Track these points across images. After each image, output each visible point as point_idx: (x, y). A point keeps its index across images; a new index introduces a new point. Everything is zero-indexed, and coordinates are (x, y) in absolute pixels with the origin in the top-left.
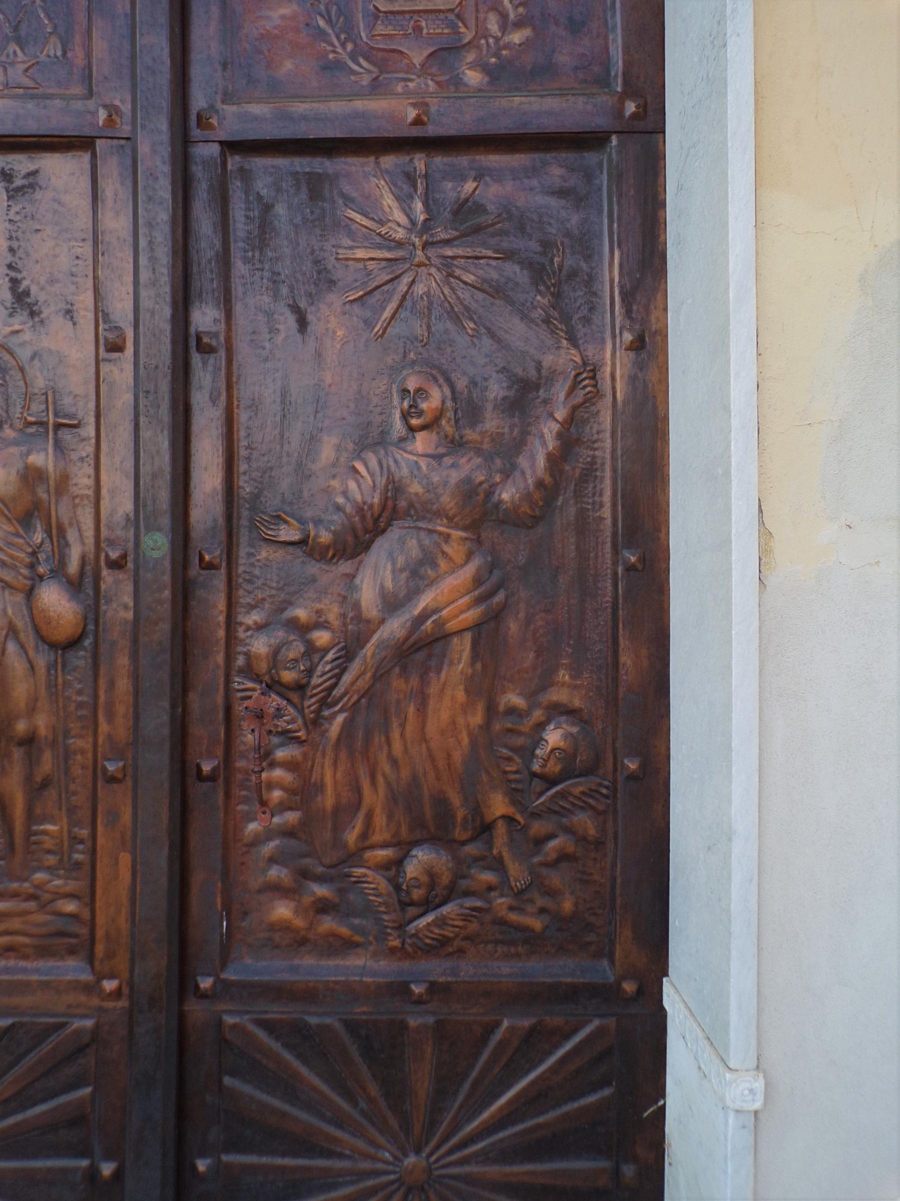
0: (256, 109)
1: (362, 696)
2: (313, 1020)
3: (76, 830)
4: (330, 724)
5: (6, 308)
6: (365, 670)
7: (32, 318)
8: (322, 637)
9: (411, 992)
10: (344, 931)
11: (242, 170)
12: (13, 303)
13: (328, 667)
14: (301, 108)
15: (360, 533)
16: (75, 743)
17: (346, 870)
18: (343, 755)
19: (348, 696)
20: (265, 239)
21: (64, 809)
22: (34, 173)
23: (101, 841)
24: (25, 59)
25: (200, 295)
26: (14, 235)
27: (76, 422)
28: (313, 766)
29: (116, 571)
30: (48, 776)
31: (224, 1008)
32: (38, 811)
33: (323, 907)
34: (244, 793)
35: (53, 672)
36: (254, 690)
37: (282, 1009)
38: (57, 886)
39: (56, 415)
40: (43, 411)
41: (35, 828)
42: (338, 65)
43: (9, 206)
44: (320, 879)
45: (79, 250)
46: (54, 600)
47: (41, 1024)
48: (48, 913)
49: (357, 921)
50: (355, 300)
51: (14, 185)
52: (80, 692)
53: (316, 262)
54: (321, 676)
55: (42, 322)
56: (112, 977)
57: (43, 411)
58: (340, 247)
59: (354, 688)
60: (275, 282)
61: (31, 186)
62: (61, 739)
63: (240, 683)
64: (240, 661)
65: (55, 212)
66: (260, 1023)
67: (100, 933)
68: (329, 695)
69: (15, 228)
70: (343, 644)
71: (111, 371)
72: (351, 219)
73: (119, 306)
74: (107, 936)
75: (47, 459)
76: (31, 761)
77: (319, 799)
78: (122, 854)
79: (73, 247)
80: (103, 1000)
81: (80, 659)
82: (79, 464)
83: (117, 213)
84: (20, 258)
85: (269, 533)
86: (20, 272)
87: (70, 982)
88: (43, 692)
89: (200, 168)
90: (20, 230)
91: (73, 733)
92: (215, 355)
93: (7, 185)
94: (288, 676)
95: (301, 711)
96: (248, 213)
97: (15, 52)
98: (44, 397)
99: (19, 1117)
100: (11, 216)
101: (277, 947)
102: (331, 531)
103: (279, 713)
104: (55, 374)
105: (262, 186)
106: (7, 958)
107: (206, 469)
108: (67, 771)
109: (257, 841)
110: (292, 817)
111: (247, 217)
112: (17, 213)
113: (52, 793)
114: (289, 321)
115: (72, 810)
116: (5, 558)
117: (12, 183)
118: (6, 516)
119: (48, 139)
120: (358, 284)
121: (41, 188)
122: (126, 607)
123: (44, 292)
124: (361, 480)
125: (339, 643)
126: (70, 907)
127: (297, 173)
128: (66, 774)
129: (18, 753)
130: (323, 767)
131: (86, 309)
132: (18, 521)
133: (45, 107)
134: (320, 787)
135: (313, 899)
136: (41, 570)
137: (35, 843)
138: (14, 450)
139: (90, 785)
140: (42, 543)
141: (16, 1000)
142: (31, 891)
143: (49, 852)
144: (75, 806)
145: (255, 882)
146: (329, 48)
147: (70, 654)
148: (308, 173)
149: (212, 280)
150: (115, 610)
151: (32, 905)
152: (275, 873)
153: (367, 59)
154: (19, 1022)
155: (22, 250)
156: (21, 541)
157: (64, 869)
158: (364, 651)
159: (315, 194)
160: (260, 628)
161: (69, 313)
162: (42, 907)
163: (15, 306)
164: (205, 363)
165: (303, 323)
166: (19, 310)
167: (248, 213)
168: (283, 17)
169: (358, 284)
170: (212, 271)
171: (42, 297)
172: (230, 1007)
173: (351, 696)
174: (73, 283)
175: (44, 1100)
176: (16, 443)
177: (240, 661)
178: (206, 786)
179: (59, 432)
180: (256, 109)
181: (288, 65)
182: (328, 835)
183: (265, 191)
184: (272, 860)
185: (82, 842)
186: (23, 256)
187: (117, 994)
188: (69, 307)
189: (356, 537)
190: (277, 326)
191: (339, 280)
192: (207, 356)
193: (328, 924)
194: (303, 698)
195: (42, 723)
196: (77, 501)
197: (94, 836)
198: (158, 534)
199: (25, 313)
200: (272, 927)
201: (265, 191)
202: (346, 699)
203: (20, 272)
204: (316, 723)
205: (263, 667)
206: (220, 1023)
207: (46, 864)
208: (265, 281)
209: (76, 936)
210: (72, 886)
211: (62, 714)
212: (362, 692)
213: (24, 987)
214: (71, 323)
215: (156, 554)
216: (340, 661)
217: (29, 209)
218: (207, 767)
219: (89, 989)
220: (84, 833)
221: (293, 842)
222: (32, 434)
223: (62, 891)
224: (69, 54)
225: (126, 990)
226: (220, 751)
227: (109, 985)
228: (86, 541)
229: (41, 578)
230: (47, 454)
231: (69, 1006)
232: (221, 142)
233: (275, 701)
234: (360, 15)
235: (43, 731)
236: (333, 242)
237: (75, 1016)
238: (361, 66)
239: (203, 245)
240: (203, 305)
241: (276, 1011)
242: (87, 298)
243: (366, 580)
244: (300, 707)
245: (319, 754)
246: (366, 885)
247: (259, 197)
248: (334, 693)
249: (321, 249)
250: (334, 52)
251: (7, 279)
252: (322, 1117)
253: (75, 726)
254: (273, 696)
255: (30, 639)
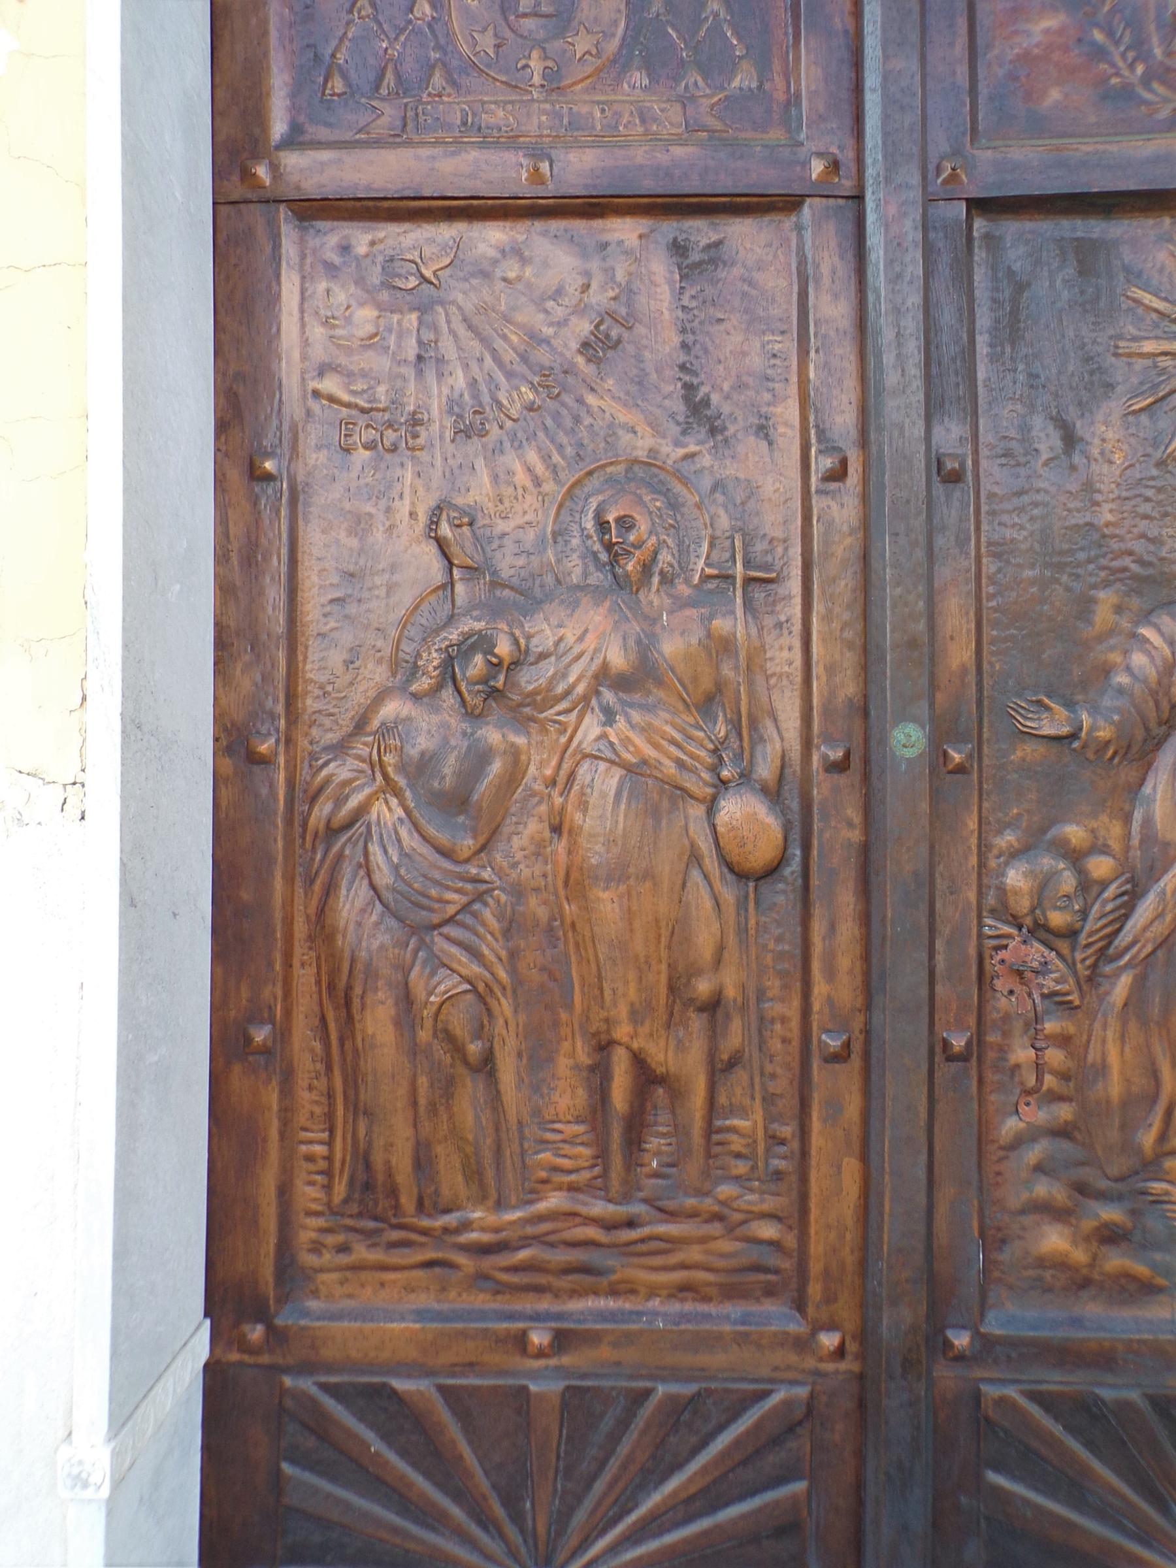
0: (1017, 154)
1: (1160, 945)
2: (1107, 1394)
3: (775, 1126)
4: (1114, 985)
5: (678, 424)
6: (1163, 910)
7: (713, 435)
8: (1100, 866)
9: (948, 1344)
10: (1141, 1269)
11: (987, 237)
12: (687, 417)
13: (1110, 907)
14: (1086, 147)
15: (1152, 724)
16: (772, 1008)
17: (1142, 1184)
18: (1133, 1026)
19: (1139, 945)
20: (1019, 329)
21: (758, 1096)
22: (718, 244)
23: (817, 1140)
24: (708, 91)
25: (942, 405)
26: (688, 326)
27: (774, 575)
28: (1088, 1042)
29: (836, 776)
30: (739, 1051)
31: (986, 1375)
32: (722, 1100)
33: (1110, 1236)
34: (997, 1077)
35: (742, 912)
36: (1009, 936)
37: (1064, 1379)
38: (749, 1203)
39: (747, 563)
40: (727, 561)
41: (718, 1123)
42: (1126, 94)
43: (681, 288)
44: (1103, 1196)
45: (777, 346)
46: (740, 810)
47: (737, 1391)
48: (737, 1239)
49: (1158, 1256)
50: (1142, 410)
51: (689, 261)
52: (779, 939)
53: (1088, 359)
54: (1100, 918)
55: (726, 441)
56: (831, 1327)
57: (727, 561)
58: (1120, 337)
59: (1148, 934)
60: (1032, 386)
61: (714, 262)
62: (753, 1002)
63: (992, 926)
64: (991, 900)
65: (744, 295)
66: (1034, 1396)
67: (815, 1268)
68: (1110, 943)
69: (690, 316)
70: (1128, 875)
71: (829, 507)
72: (1135, 300)
73: (839, 419)
74: (826, 1272)
75: (735, 626)
76: (714, 1034)
77: (1100, 1085)
78: (846, 1160)
79: (768, 343)
80: (821, 1360)
81: (782, 895)
82: (775, 633)
83: (836, 296)
84: (697, 357)
85: (1029, 724)
86: (697, 375)
87: (775, 1334)
88: (732, 939)
89: (941, 235)
90: (697, 321)
91: (770, 994)
92: (962, 485)
93: (680, 260)
94: (1057, 919)
95: (1072, 966)
96: (996, 295)
97: (696, 83)
98: (730, 540)
99: (705, 1523)
100: (685, 302)
101: (1049, 1290)
102: (1112, 723)
103: (1043, 969)
104: (744, 511)
105: (1016, 257)
106: (683, 1300)
107: (952, 638)
108: (762, 1044)
109: (1018, 1142)
110: (1065, 1112)
111: (994, 300)
112: (693, 297)
113: (740, 1075)
114: (1048, 441)
115: (769, 1099)
116: (685, 758)
117: (687, 257)
118: (684, 700)
119: (744, 199)
120: (1145, 388)
121: (725, 264)
122: (850, 825)
123: (729, 402)
124: (1153, 652)
125: (1123, 874)
126: (768, 1231)
127: (1063, 238)
128: (760, 1050)
129: (697, 1022)
130: (1104, 1042)
131: (786, 424)
132: (696, 708)
133: (741, 157)
134: (1102, 1069)
135: (1096, 1224)
136: (725, 773)
137: (719, 1144)
138: (693, 612)
139: (796, 1065)
140: (726, 737)
141: (703, 1359)
142: (716, 1208)
143: (738, 1156)
144: (773, 1094)
145: (1015, 1198)
146: (1111, 71)
147: (765, 887)
148: (1077, 239)
149: (958, 384)
150: (835, 827)
151: (716, 1228)
152: (1043, 1189)
153: (1163, 82)
154: (706, 1389)
155: (698, 346)
156: (701, 734)
157: (758, 1180)
158: (1162, 883)
159: (1085, 270)
160: (1014, 855)
161: (763, 430)
162: (731, 1229)
163: (691, 420)
164: (948, 496)
165: (1070, 440)
166: (695, 426)
167: (996, 295)
168: (1047, 31)
169: (1145, 388)
170: (957, 374)
171: (726, 409)
172: (996, 1375)
173: (1144, 946)
174: (768, 390)
175: (742, 1498)
176: (691, 603)
177: (991, 900)
178: (955, 1066)
179: (750, 589)
180: (1017, 154)
181: (1055, 95)
182: (1114, 1135)
183: (1019, 264)
184: (1039, 1168)
185: (783, 1142)
186: (700, 353)
187: (840, 1352)
188: (763, 421)
189: (1147, 729)
190: (1036, 446)
191: (1118, 384)
192: (951, 485)
193: (1116, 1261)
194: (1073, 949)
195: (730, 981)
196: (773, 681)
197: (804, 1132)
198: (911, 725)
199: (703, 430)
200: (1041, 1262)
201: (1019, 264)
202: (1135, 949)
203: (697, 375)
204: (1093, 979)
205: (1023, 905)
206: (977, 1396)
207: (735, 1172)
208: (1019, 385)
209: (777, 1272)
210: (770, 1203)
211: (754, 966)
212: (1159, 940)
213: (712, 1341)
214: (765, 443)
215: (910, 753)
216: (1126, 898)
217: (710, 291)
218: (958, 1042)
219: (803, 1344)
220: (787, 1131)
221: (1066, 1145)
222: (711, 592)
223: (756, 1209)
224: (767, 86)
225: (852, 1347)
226: (972, 1021)
227: (829, 1340)
228: (786, 735)
229: (724, 782)
230: (736, 619)
231: (776, 1369)
232: (967, 200)
233: (1036, 952)
234: (1152, 27)
235: (731, 992)
236: (1111, 332)
237: (782, 1381)
238: (1156, 94)
239: (945, 338)
240: (946, 419)
241: (1055, 1381)
242: (789, 411)
243: (1160, 789)
244: (1070, 961)
245: (1097, 1025)
246: (1169, 1206)
247: (1010, 273)
248: (1116, 943)
249: (1094, 342)
250: (1117, 74)
251: (679, 385)
252: (1119, 1527)
253: (773, 985)
254: (1036, 944)
255: (711, 863)
